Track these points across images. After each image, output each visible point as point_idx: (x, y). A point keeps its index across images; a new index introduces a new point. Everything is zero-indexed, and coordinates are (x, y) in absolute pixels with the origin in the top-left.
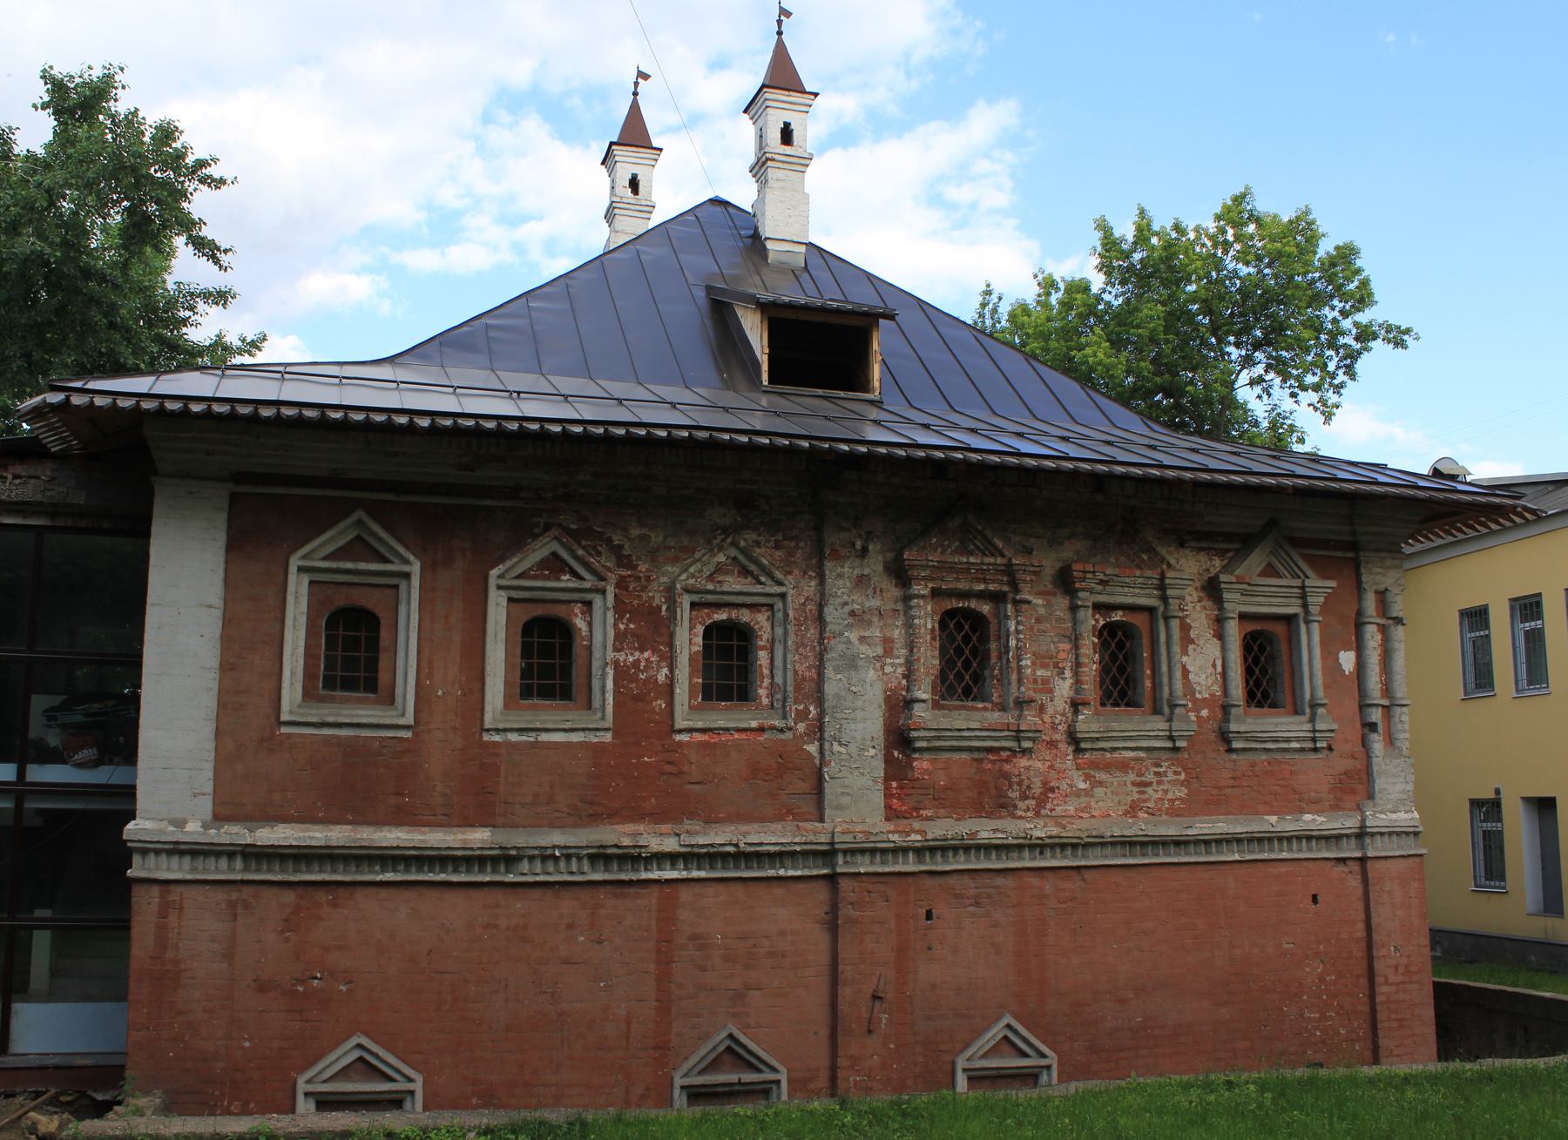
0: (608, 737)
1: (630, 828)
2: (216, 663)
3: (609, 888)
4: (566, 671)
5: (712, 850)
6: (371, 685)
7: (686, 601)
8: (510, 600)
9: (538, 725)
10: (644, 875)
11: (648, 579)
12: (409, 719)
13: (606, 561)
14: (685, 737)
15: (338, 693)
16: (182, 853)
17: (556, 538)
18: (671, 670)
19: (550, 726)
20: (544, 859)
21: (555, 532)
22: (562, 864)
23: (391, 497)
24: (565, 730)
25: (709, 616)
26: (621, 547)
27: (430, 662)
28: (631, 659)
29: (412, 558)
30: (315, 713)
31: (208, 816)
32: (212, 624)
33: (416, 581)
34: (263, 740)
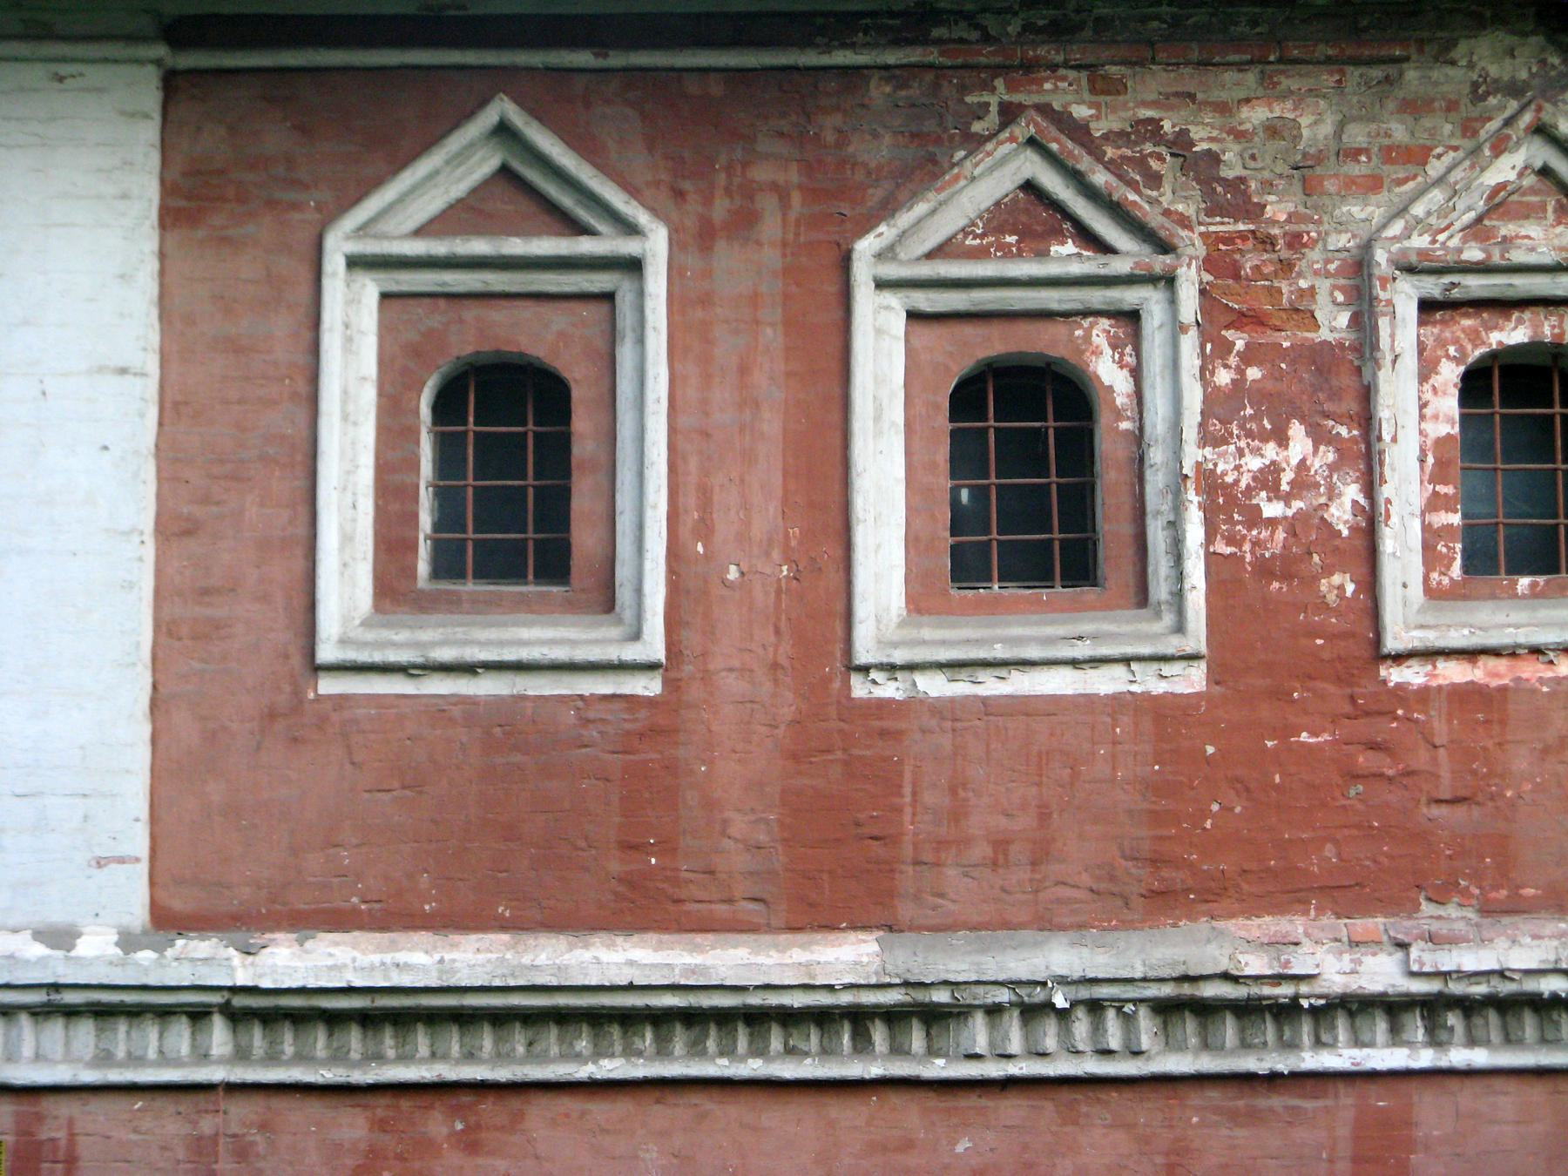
0: (1192, 680)
1: (1269, 925)
2: (147, 521)
3: (1214, 1094)
4: (1080, 505)
5: (1505, 988)
6: (554, 564)
7: (1404, 296)
8: (914, 316)
9: (1000, 652)
10: (1312, 1060)
11: (1295, 241)
12: (654, 646)
13: (1172, 199)
14: (1411, 675)
15: (470, 587)
16: (71, 1013)
17: (1032, 142)
18: (1370, 489)
19: (1033, 653)
20: (1033, 1012)
21: (1023, 129)
22: (1081, 1027)
23: (583, 58)
24: (1074, 663)
25: (1476, 339)
26: (1214, 158)
27: (705, 495)
28: (1254, 463)
29: (643, 218)
30: (405, 640)
31: (137, 912)
32: (130, 416)
33: (657, 282)
34: (272, 715)
